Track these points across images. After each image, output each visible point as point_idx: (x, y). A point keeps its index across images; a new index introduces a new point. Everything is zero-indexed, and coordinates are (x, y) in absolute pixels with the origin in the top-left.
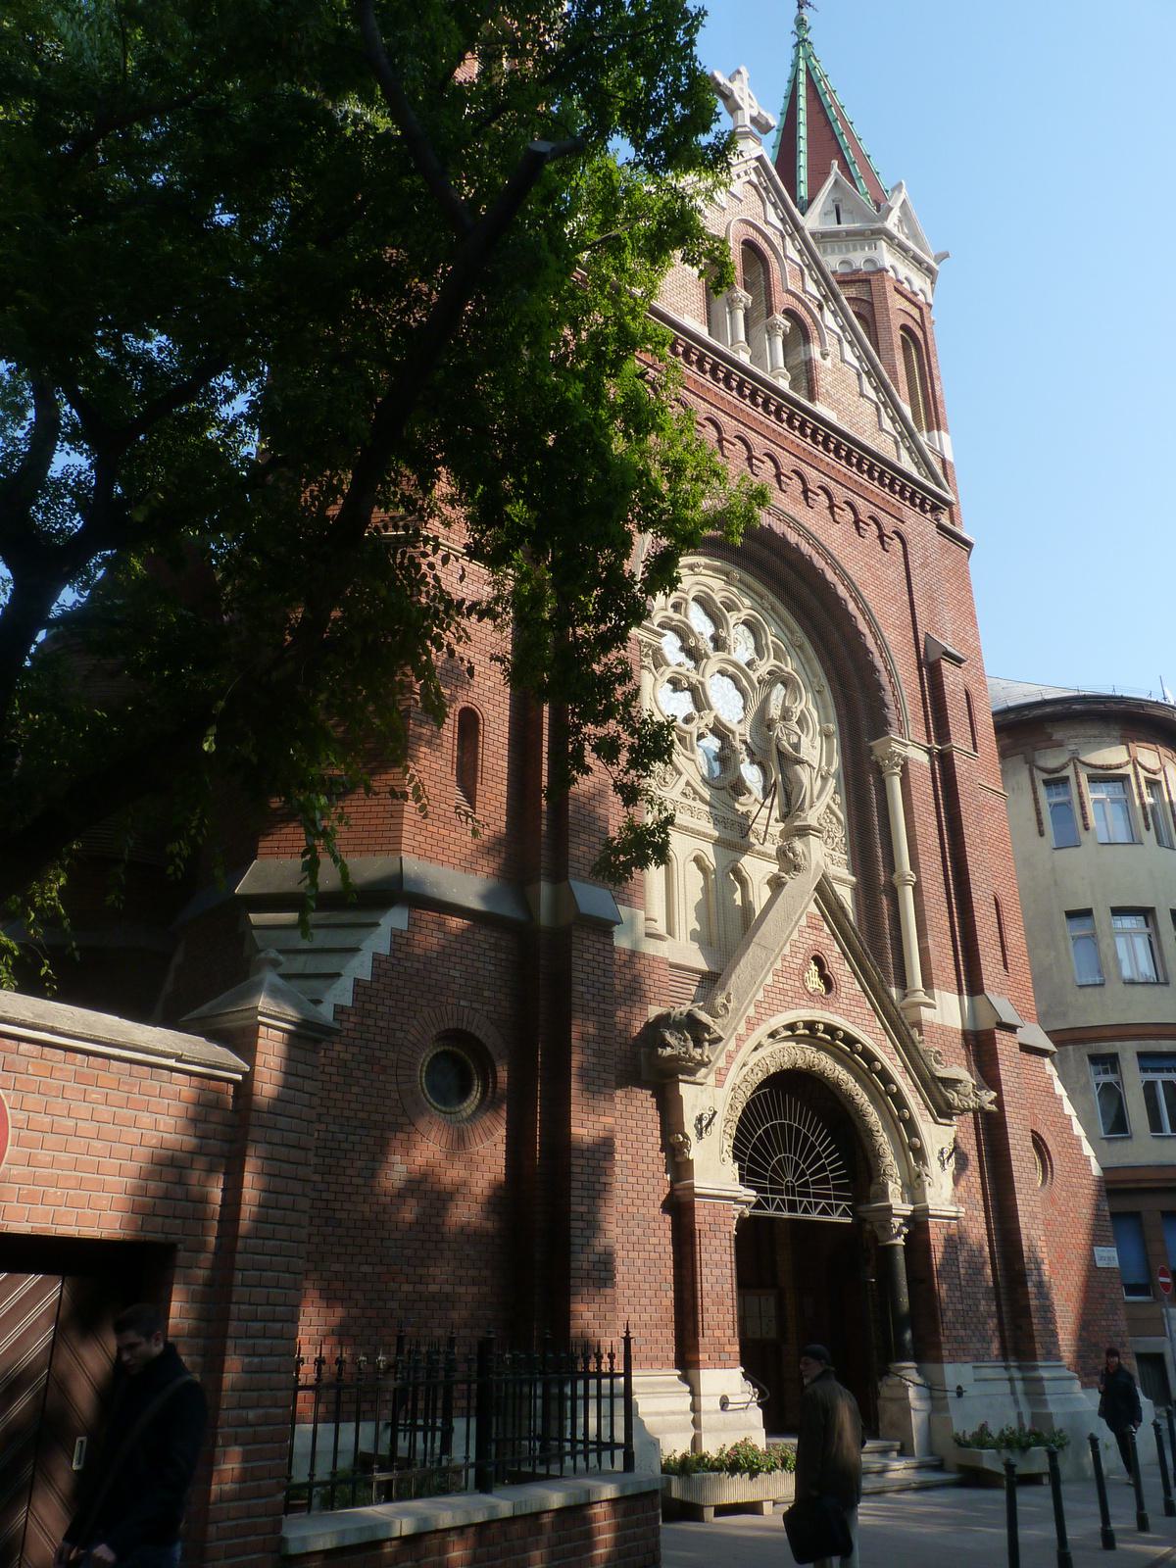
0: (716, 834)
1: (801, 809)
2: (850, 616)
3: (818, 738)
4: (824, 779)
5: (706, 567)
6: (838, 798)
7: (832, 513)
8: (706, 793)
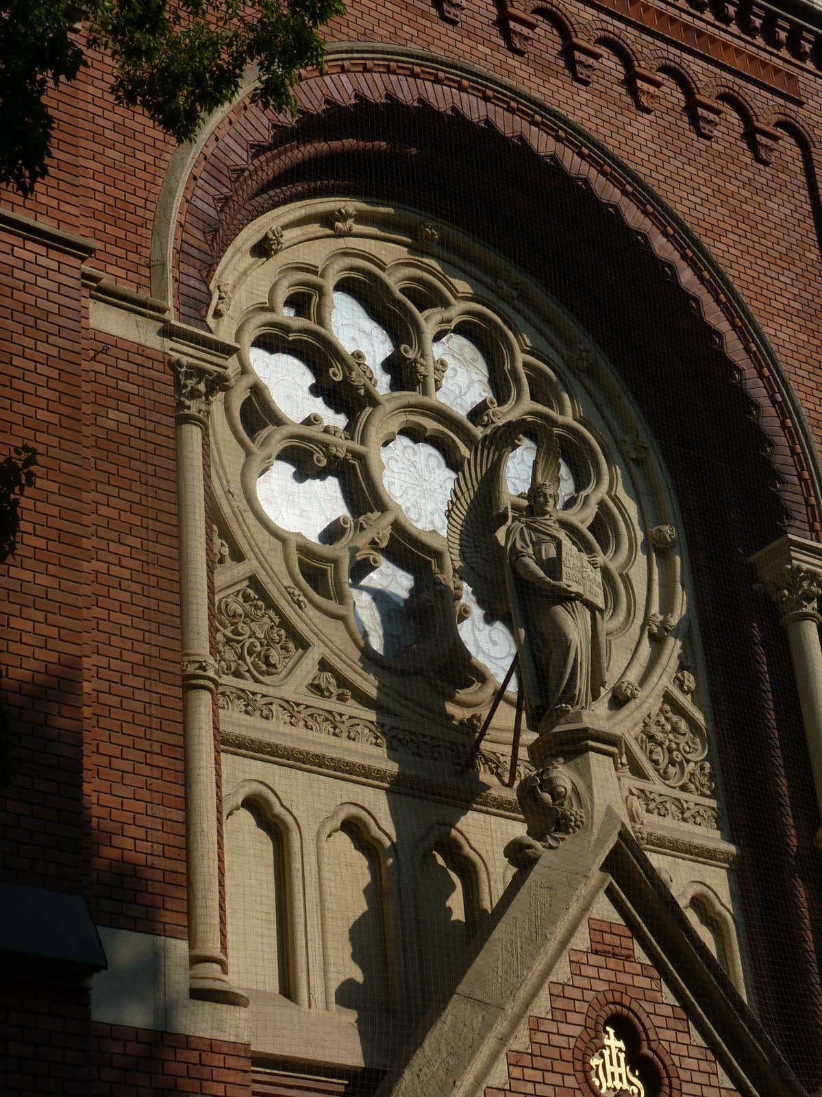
0: (393, 767)
1: (569, 696)
2: (686, 299)
3: (641, 559)
4: (658, 641)
5: (361, 218)
6: (690, 680)
7: (634, 92)
8: (369, 685)
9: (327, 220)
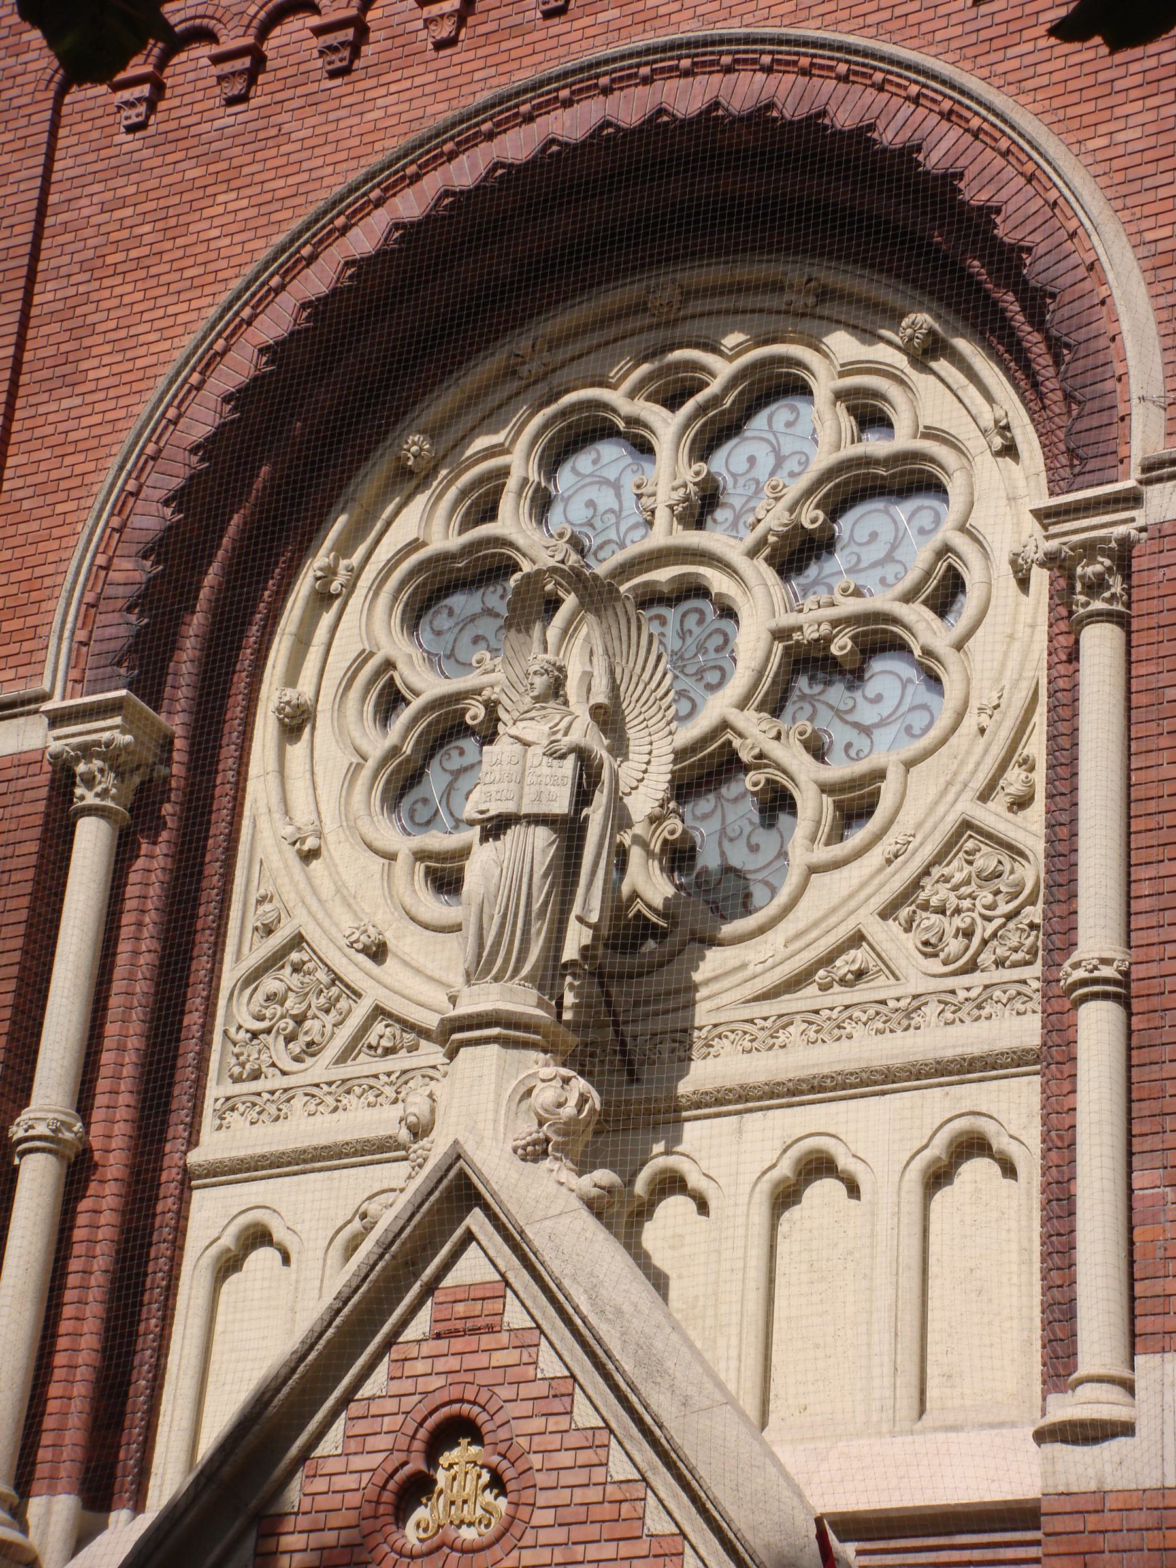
5: (344, 548)
9: (323, 598)
